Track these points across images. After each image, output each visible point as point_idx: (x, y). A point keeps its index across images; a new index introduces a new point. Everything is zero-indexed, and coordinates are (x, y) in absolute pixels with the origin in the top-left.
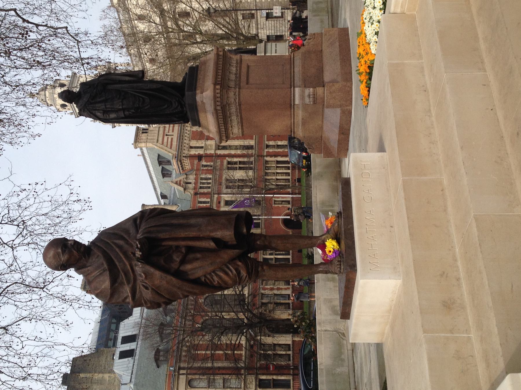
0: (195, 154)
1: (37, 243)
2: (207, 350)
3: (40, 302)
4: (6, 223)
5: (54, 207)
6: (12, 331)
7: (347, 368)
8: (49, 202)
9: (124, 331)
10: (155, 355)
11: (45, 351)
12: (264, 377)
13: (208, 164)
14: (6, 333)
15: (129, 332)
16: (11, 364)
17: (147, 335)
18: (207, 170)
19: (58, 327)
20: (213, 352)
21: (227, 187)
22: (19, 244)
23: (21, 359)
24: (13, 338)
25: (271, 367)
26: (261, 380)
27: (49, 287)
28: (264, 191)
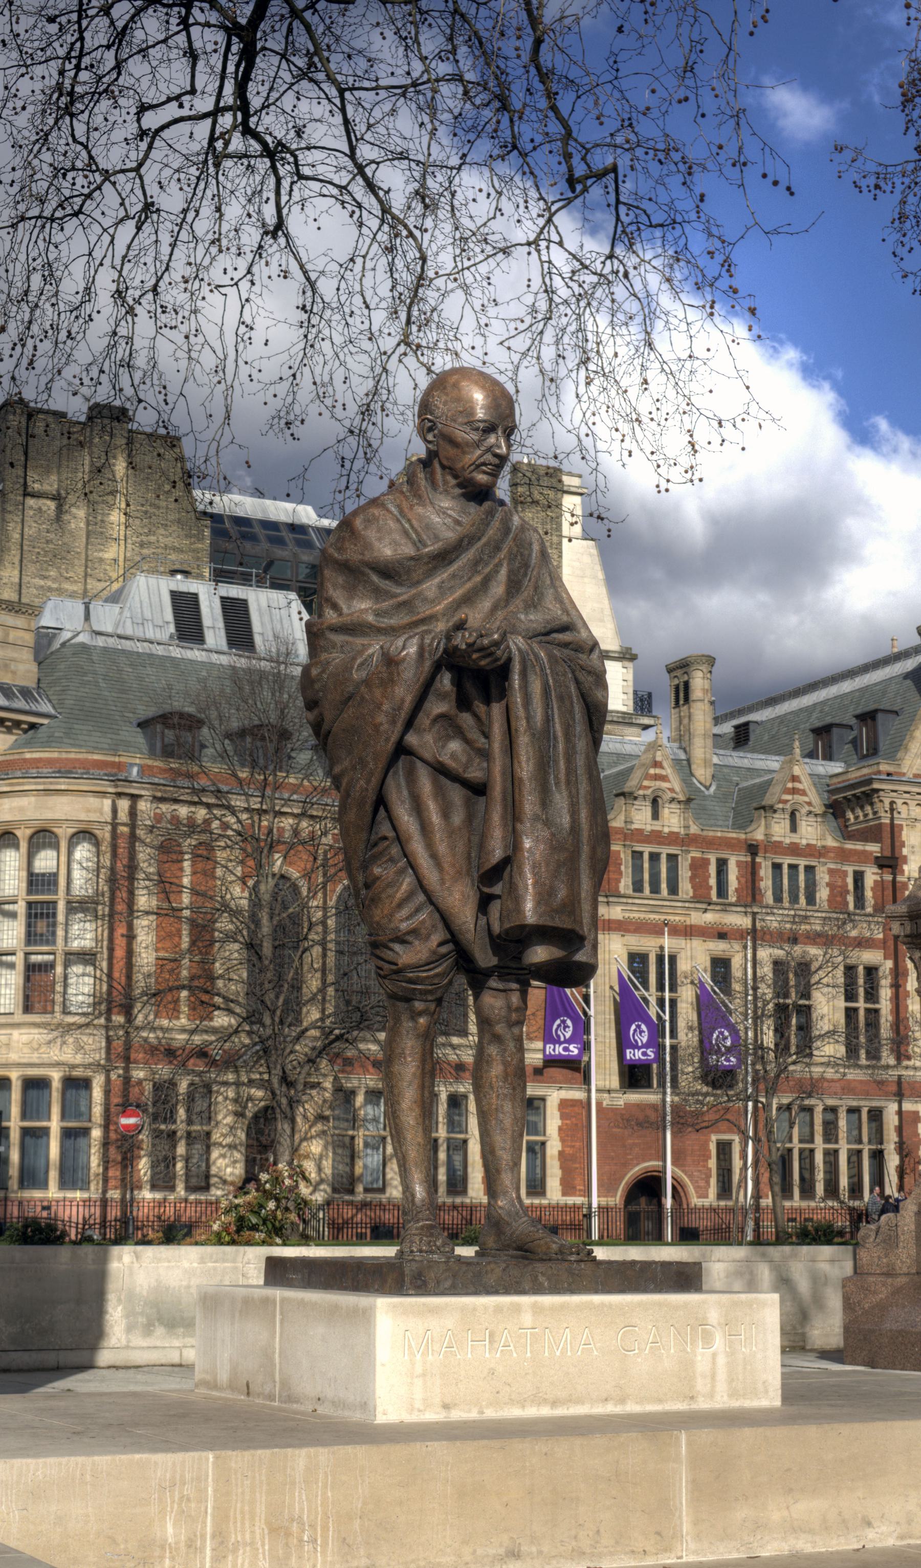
0: (903, 845)
1: (550, 318)
2: (194, 892)
3: (361, 337)
4: (618, 219)
5: (674, 368)
6: (270, 251)
7: (124, 1342)
8: (688, 352)
9: (264, 604)
10: (181, 715)
11: (207, 354)
12: (97, 1094)
13: (869, 894)
14: (266, 233)
15: (262, 624)
16: (165, 249)
17: (251, 683)
18: (845, 892)
19: (281, 395)
20: (186, 913)
21: (778, 965)
22: (550, 262)
23: (184, 286)
24: (250, 257)
25: (132, 1121)
26: (86, 1084)
27: (410, 360)
28: (763, 1100)
